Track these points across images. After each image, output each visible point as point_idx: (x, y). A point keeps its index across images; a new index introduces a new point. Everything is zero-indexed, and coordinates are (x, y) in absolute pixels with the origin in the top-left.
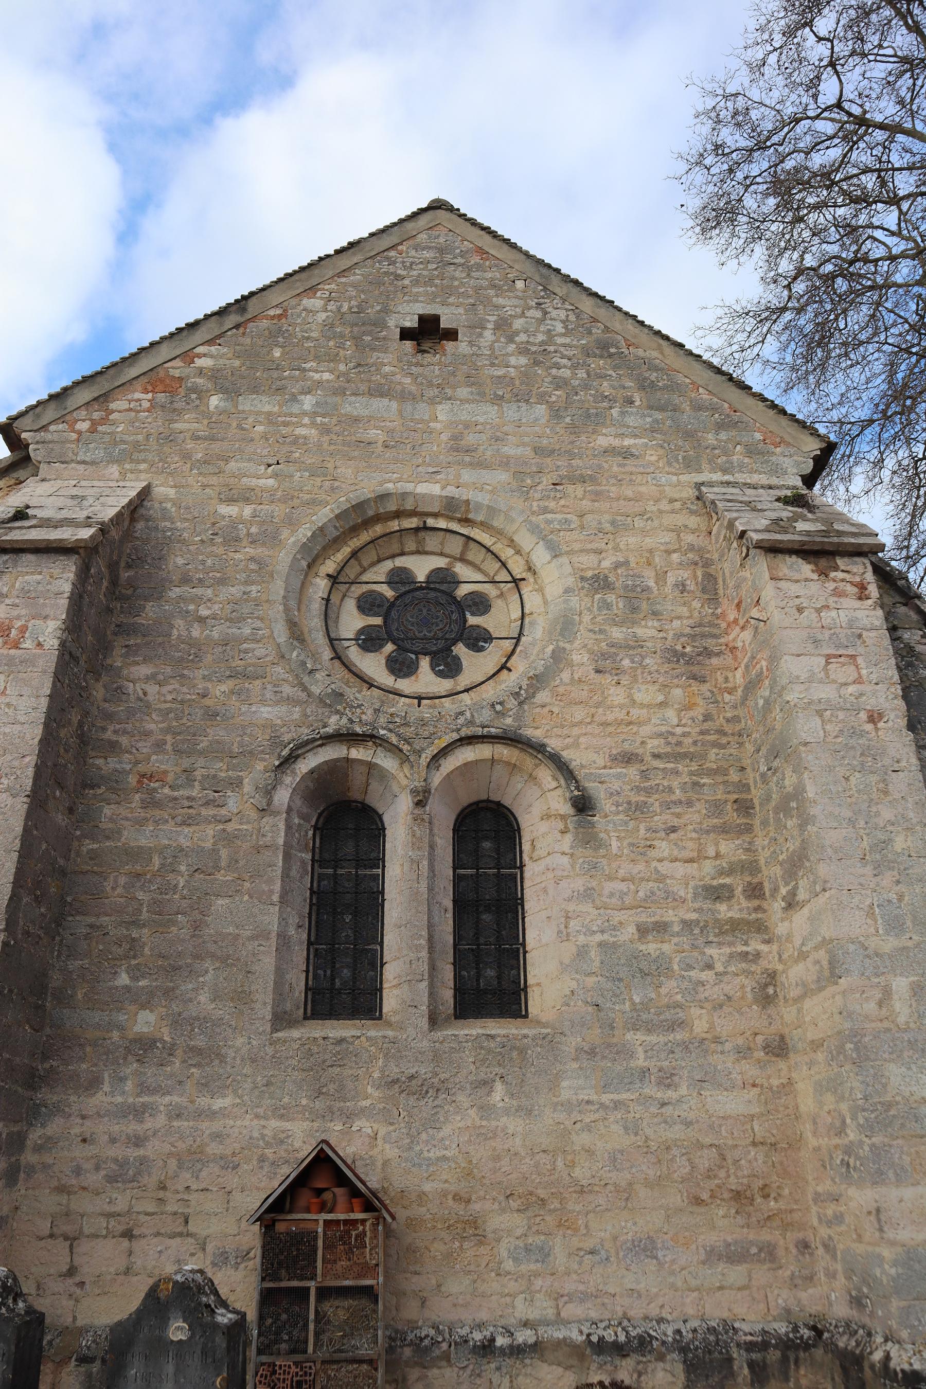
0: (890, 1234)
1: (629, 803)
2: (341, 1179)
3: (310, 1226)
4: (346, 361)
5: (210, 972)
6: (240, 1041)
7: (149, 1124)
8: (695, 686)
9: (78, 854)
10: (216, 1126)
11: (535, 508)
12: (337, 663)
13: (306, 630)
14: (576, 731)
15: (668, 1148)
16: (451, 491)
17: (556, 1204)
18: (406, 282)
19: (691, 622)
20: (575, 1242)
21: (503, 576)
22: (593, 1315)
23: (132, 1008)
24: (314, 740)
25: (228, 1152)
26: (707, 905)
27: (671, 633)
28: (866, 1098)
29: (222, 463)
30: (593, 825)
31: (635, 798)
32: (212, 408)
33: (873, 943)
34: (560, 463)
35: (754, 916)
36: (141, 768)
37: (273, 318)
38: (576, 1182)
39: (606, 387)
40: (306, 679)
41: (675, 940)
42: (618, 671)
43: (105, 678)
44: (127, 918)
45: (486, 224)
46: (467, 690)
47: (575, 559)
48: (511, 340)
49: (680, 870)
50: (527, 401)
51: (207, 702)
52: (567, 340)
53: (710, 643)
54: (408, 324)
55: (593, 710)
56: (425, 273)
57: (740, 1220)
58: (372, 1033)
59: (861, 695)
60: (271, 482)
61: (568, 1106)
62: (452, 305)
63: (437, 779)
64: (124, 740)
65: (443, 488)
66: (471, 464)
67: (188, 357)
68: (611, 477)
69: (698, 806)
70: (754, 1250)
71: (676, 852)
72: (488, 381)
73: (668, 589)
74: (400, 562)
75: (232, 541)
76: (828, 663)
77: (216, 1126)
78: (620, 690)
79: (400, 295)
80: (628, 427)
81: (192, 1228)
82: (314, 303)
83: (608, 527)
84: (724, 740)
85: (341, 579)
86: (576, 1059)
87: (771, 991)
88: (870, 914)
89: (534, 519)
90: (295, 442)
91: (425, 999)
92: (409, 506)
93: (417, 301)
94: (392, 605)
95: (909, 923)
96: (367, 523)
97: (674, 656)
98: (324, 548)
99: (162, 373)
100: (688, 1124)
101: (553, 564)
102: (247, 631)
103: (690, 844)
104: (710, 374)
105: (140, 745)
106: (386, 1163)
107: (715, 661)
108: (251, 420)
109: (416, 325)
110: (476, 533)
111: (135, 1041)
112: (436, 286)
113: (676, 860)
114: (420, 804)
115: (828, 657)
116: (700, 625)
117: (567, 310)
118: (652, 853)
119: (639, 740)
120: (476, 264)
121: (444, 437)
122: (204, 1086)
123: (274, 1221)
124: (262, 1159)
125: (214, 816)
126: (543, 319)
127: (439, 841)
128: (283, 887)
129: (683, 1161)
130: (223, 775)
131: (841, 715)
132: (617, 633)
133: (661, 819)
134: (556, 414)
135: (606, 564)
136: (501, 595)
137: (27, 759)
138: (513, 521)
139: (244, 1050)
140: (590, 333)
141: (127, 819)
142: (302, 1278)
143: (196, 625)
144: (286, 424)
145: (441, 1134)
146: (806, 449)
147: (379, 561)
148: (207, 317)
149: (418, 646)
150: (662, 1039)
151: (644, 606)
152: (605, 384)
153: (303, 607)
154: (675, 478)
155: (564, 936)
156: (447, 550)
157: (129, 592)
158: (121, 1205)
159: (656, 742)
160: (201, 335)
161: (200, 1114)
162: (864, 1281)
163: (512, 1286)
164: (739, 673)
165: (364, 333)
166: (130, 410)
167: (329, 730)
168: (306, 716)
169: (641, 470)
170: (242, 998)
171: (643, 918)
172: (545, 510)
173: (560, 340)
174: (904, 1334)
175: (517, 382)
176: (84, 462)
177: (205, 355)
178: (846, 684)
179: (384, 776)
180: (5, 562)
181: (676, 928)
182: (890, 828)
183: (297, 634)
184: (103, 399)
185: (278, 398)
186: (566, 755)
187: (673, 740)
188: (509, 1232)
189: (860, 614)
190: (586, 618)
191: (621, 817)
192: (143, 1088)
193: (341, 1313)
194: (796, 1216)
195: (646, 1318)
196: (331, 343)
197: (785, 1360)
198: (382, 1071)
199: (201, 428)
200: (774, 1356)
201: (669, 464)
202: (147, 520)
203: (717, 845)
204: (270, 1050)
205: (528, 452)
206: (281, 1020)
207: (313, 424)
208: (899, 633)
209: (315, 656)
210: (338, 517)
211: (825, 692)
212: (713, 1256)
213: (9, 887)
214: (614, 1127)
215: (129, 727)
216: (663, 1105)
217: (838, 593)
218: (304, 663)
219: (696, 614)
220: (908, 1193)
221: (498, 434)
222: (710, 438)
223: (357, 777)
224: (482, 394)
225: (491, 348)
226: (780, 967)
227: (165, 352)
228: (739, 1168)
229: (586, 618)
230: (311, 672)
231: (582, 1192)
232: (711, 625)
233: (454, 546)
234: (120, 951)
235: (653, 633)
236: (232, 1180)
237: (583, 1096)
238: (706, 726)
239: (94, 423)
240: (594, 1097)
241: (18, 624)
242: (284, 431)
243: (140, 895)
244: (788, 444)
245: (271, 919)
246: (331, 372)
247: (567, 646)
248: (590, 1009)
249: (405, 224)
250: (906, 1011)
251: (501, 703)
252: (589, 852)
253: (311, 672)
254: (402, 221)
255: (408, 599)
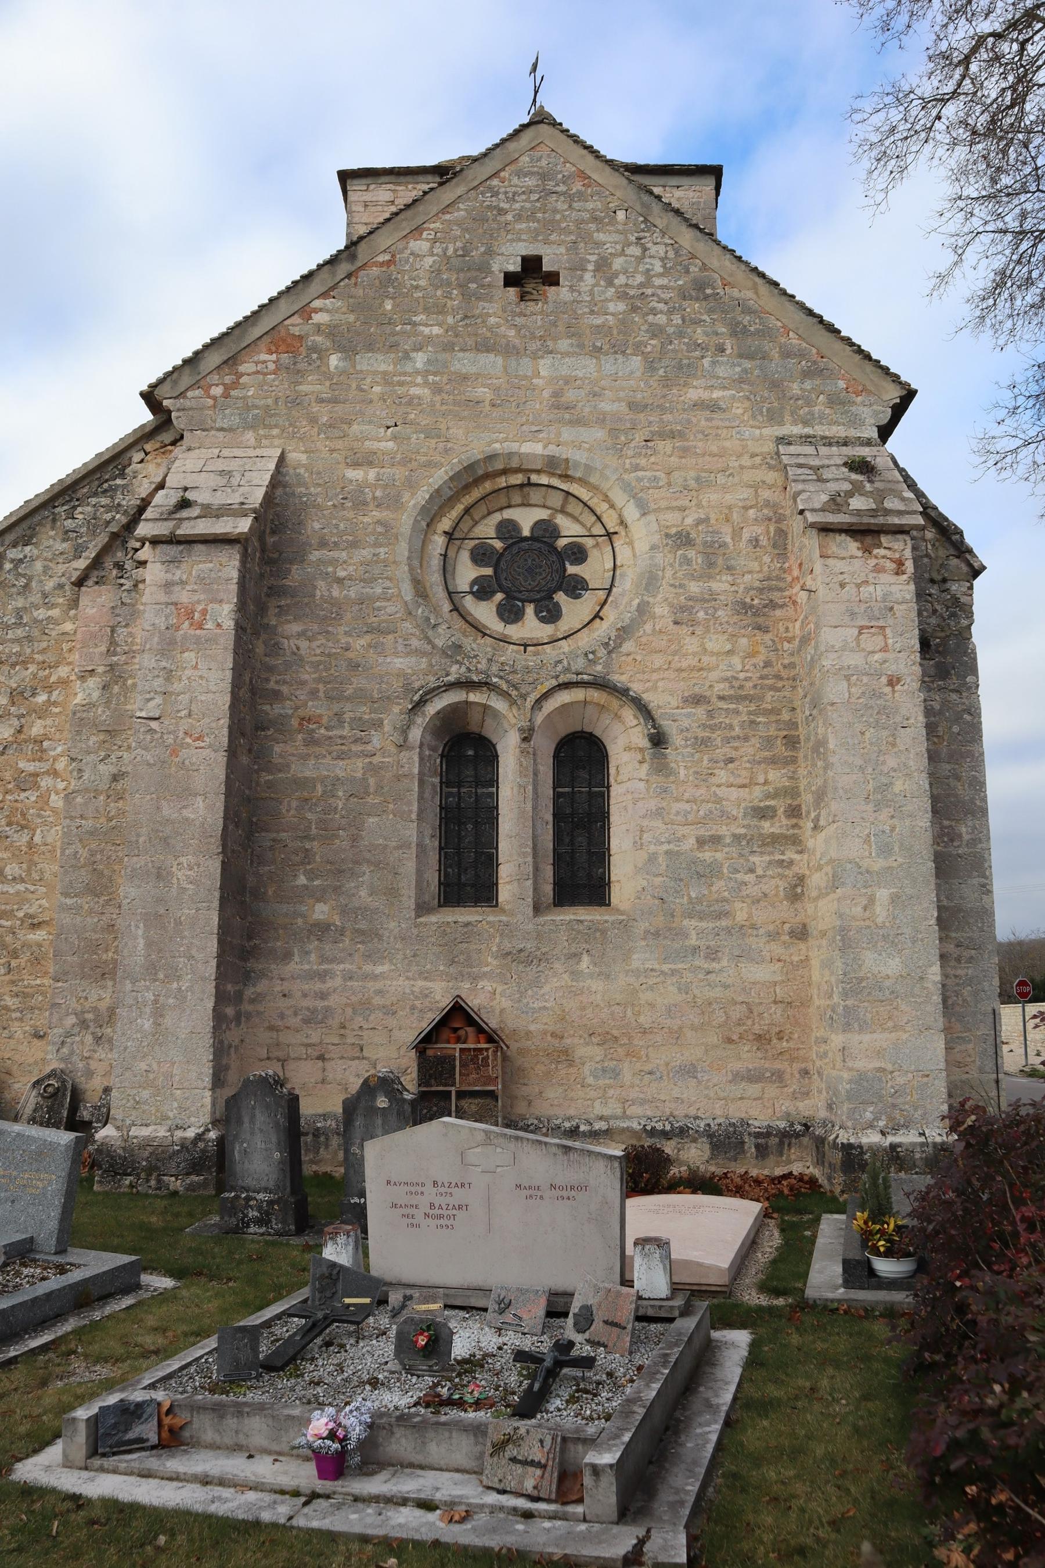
0: (850, 1064)
1: (696, 738)
2: (470, 1021)
3: (450, 1052)
4: (454, 312)
5: (367, 874)
6: (392, 925)
7: (329, 984)
8: (759, 636)
9: (258, 784)
10: (379, 985)
11: (627, 466)
12: (455, 613)
13: (428, 585)
14: (655, 676)
15: (710, 1004)
16: (552, 450)
17: (625, 1041)
18: (509, 217)
19: (761, 576)
20: (638, 1066)
21: (598, 530)
22: (649, 1113)
23: (311, 901)
24: (439, 687)
25: (388, 1003)
26: (755, 822)
27: (742, 586)
28: (845, 974)
29: (345, 426)
30: (665, 756)
31: (702, 734)
32: (332, 368)
33: (865, 863)
34: (652, 419)
35: (791, 831)
36: (301, 712)
37: (382, 264)
38: (640, 1026)
39: (699, 335)
40: (430, 633)
41: (726, 850)
42: (693, 623)
43: (264, 636)
44: (300, 834)
45: (589, 143)
46: (565, 638)
47: (661, 517)
48: (610, 283)
49: (734, 794)
50: (624, 352)
51: (350, 655)
52: (664, 281)
53: (775, 596)
54: (511, 268)
55: (670, 658)
56: (528, 205)
57: (759, 1054)
58: (491, 918)
59: (885, 661)
60: (391, 444)
61: (637, 973)
62: (554, 243)
63: (539, 718)
64: (285, 689)
65: (545, 447)
66: (570, 422)
67: (306, 312)
68: (698, 432)
69: (753, 741)
70: (768, 1074)
71: (731, 779)
72: (588, 331)
73: (742, 545)
74: (508, 514)
75: (360, 505)
76: (860, 633)
77: (379, 985)
78: (694, 640)
79: (503, 233)
80: (718, 378)
81: (366, 1053)
82: (420, 245)
83: (692, 484)
84: (780, 684)
85: (456, 535)
86: (644, 939)
87: (799, 890)
88: (867, 841)
89: (626, 476)
90: (410, 403)
91: (531, 893)
92: (514, 464)
93: (520, 240)
94: (502, 554)
95: (896, 849)
96: (478, 481)
97: (744, 608)
98: (440, 508)
99: (283, 333)
100: (726, 987)
101: (641, 522)
102: (379, 590)
103: (744, 773)
104: (801, 316)
105: (298, 693)
106: (502, 1011)
107: (778, 613)
108: (369, 380)
109: (519, 269)
110: (575, 489)
111: (314, 925)
112: (538, 221)
113: (732, 786)
114: (525, 739)
115: (862, 628)
116: (769, 579)
117: (666, 245)
118: (713, 780)
119: (708, 684)
120: (579, 192)
121: (546, 394)
122: (368, 957)
123: (425, 1049)
124: (413, 1008)
125: (362, 751)
126: (643, 257)
127: (541, 768)
128: (419, 808)
129: (721, 1013)
130: (367, 717)
131: (865, 679)
132: (694, 588)
133: (720, 753)
134: (651, 366)
135: (689, 521)
136: (597, 544)
137: (222, 722)
138: (607, 479)
139: (397, 930)
140: (687, 272)
141: (293, 755)
142: (446, 1085)
143: (335, 586)
144: (401, 384)
145: (542, 991)
146: (886, 397)
147: (489, 513)
148: (320, 267)
149: (525, 595)
150: (711, 925)
151: (720, 561)
152: (699, 330)
153: (425, 563)
154: (758, 432)
155: (638, 845)
156: (549, 503)
157: (276, 556)
158: (315, 1038)
159: (722, 686)
160: (316, 287)
161: (366, 977)
162: (834, 1094)
163: (593, 1094)
164: (798, 624)
165: (471, 280)
166: (258, 372)
167: (451, 678)
168: (431, 665)
169: (727, 424)
170: (392, 893)
171: (702, 832)
172: (637, 468)
173: (658, 282)
174: (849, 1124)
175: (615, 332)
176: (222, 429)
177: (321, 310)
178: (873, 652)
179: (496, 714)
180: (181, 552)
181: (728, 840)
182: (892, 774)
183: (421, 592)
184: (231, 362)
185: (393, 356)
186: (646, 697)
187: (736, 684)
188: (591, 1058)
189: (894, 589)
190: (669, 573)
191: (689, 749)
192: (323, 959)
193: (473, 1107)
194: (801, 1053)
195: (686, 1116)
196: (439, 293)
197: (781, 1143)
198: (499, 946)
199: (323, 389)
200: (774, 1141)
201: (754, 417)
202: (285, 487)
203: (766, 773)
204: (415, 931)
205: (623, 407)
206: (422, 909)
207: (426, 383)
208: (948, 585)
209: (436, 610)
210: (451, 479)
211: (854, 660)
212: (737, 1077)
213: (221, 821)
214: (671, 988)
215: (288, 678)
216: (709, 973)
217: (878, 569)
218: (428, 619)
219: (766, 569)
220: (866, 1038)
221: (596, 389)
222: (795, 388)
223: (475, 716)
224: (581, 346)
225: (591, 293)
226: (807, 873)
227: (284, 308)
228: (763, 1018)
229: (669, 573)
230: (435, 626)
231: (645, 1033)
232: (779, 578)
233: (556, 500)
234: (297, 859)
235: (725, 586)
236: (392, 1022)
237: (648, 966)
238: (766, 671)
239: (227, 388)
240: (657, 967)
241: (200, 608)
242: (400, 390)
243: (309, 816)
244: (870, 393)
245: (411, 832)
246: (440, 325)
247: (651, 600)
248: (657, 902)
249: (507, 144)
250: (884, 914)
251: (593, 653)
252: (661, 779)
253: (435, 626)
254: (504, 141)
255: (515, 549)
